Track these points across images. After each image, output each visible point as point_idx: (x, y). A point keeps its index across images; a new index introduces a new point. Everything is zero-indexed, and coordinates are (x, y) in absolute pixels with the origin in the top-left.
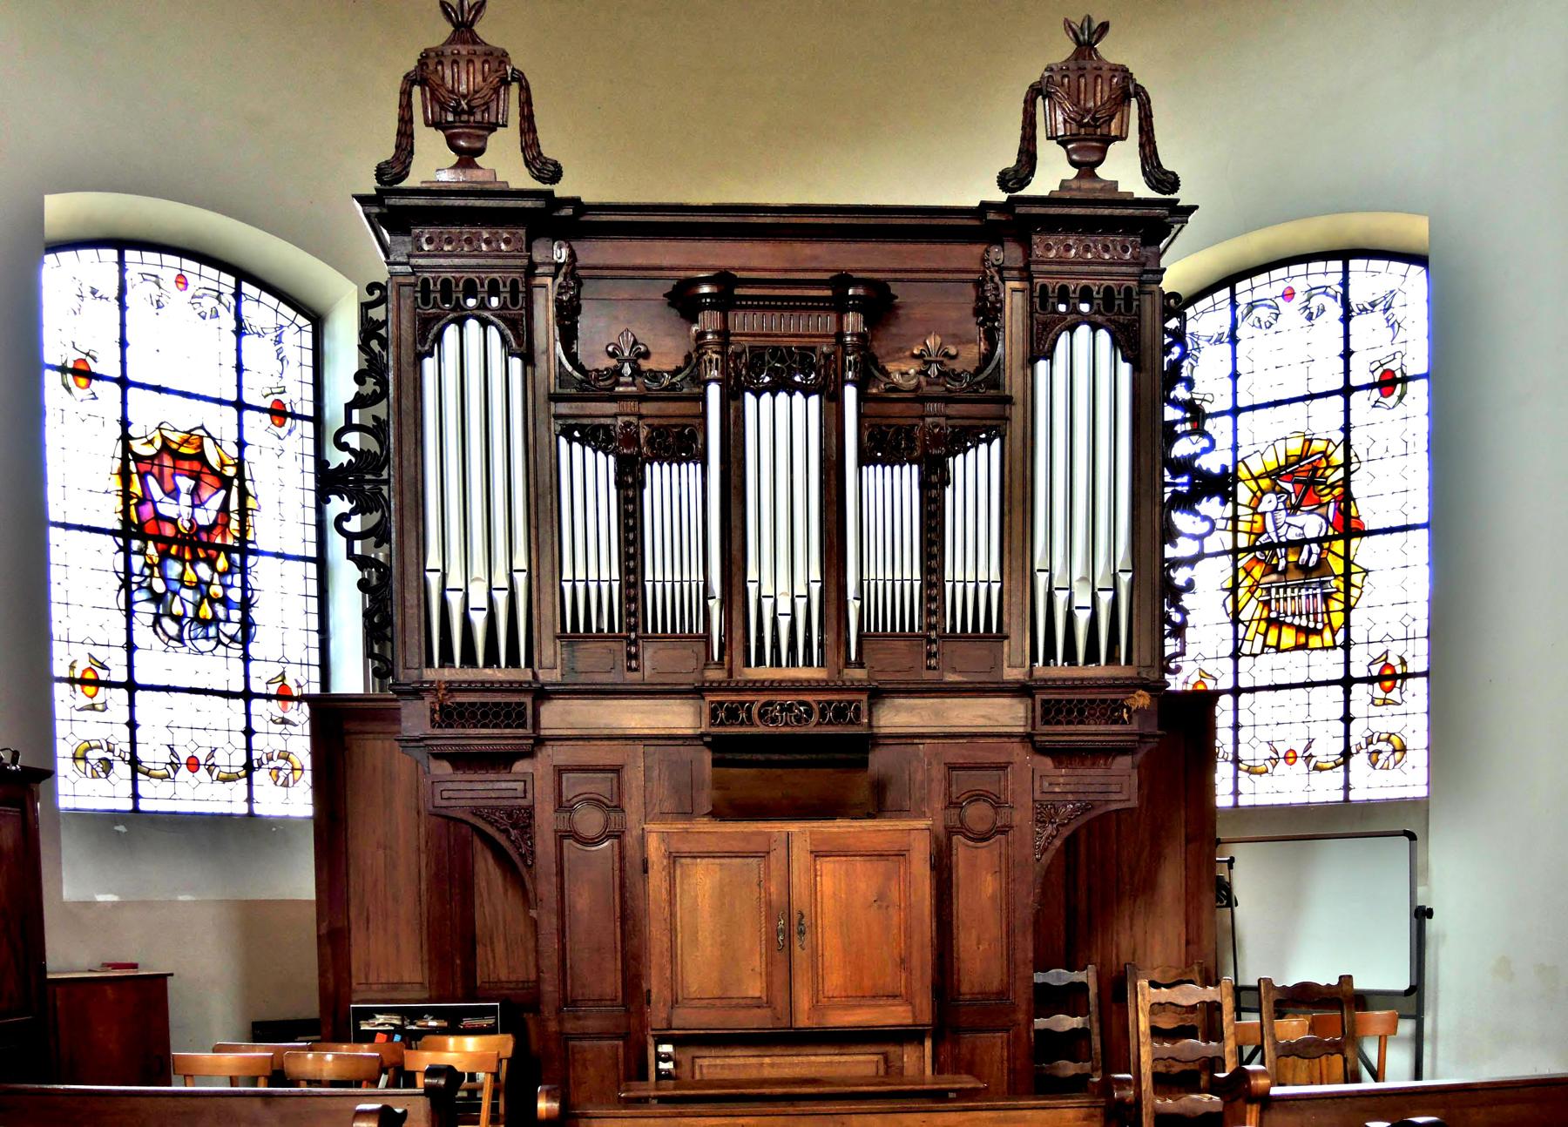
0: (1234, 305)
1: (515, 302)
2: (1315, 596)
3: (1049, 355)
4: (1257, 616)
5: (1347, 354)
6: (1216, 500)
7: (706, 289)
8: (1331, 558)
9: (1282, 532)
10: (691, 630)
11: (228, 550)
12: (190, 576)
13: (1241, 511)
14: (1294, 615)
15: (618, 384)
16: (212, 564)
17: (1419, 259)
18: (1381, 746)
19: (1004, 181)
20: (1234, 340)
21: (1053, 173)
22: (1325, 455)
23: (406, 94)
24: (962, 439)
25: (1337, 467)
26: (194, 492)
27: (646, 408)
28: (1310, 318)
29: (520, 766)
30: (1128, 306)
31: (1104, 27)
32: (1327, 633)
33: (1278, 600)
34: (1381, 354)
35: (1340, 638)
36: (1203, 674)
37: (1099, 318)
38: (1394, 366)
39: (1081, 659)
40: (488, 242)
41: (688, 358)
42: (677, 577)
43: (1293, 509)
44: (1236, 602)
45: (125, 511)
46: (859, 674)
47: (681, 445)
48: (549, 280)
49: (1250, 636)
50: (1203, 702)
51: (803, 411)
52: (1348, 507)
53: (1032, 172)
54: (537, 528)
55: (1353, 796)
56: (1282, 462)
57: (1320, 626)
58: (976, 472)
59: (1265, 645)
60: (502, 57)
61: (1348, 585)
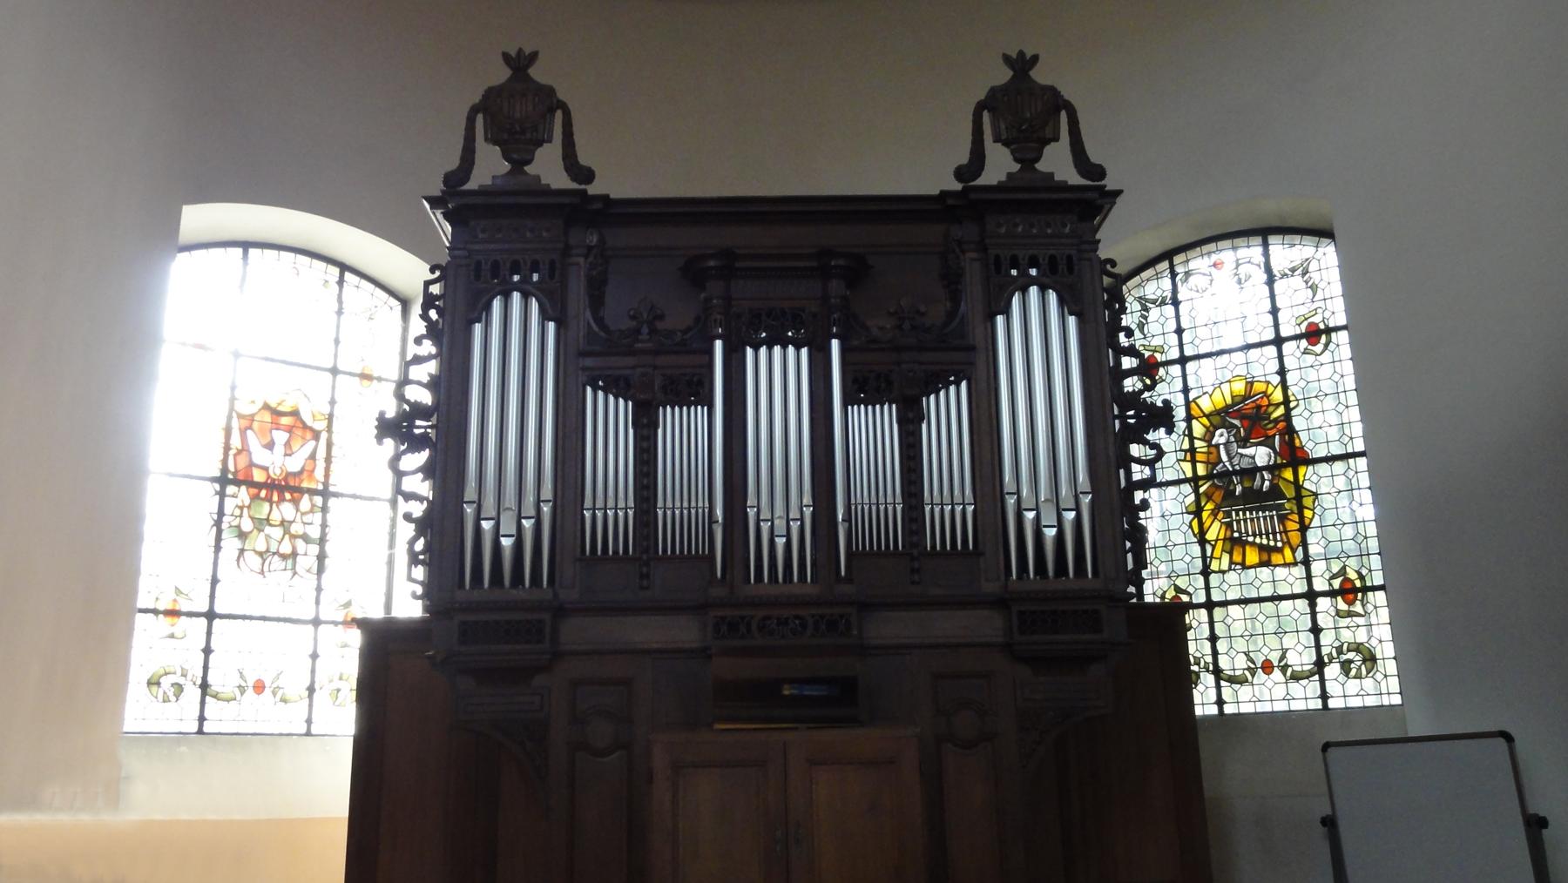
0: (1174, 275)
1: (552, 277)
2: (1272, 517)
3: (1007, 311)
4: (1222, 536)
5: (1274, 311)
6: (1162, 430)
7: (712, 263)
8: (1282, 484)
9: (1236, 461)
10: (665, 550)
11: (312, 492)
12: (276, 517)
13: (1198, 444)
14: (1254, 535)
15: (638, 341)
16: (296, 502)
17: (1323, 233)
18: (1351, 655)
19: (960, 174)
20: (1176, 303)
21: (999, 165)
22: (1265, 394)
23: (471, 121)
24: (936, 382)
25: (1278, 405)
26: (288, 444)
27: (661, 360)
28: (1239, 282)
29: (539, 680)
30: (1071, 270)
31: (1035, 58)
32: (1287, 552)
33: (1238, 522)
34: (1303, 310)
35: (1300, 554)
36: (1178, 590)
37: (1045, 280)
38: (1317, 319)
39: (1051, 572)
40: (532, 230)
41: (697, 319)
42: (685, 504)
43: (1244, 443)
44: (1201, 524)
45: (225, 462)
46: (847, 589)
47: (694, 391)
48: (581, 260)
49: (1217, 553)
50: (1172, 614)
51: (796, 360)
52: (1292, 440)
53: (982, 168)
54: (564, 463)
55: (1332, 704)
56: (1229, 401)
57: (1279, 544)
58: (947, 411)
59: (1231, 562)
60: (550, 91)
61: (1301, 508)
